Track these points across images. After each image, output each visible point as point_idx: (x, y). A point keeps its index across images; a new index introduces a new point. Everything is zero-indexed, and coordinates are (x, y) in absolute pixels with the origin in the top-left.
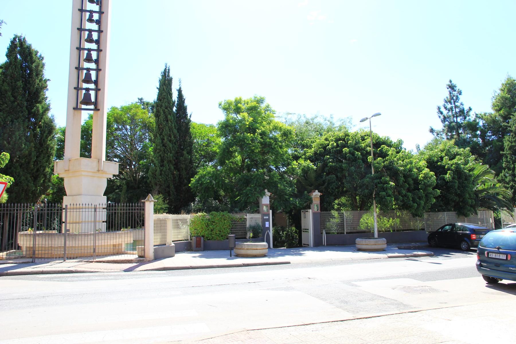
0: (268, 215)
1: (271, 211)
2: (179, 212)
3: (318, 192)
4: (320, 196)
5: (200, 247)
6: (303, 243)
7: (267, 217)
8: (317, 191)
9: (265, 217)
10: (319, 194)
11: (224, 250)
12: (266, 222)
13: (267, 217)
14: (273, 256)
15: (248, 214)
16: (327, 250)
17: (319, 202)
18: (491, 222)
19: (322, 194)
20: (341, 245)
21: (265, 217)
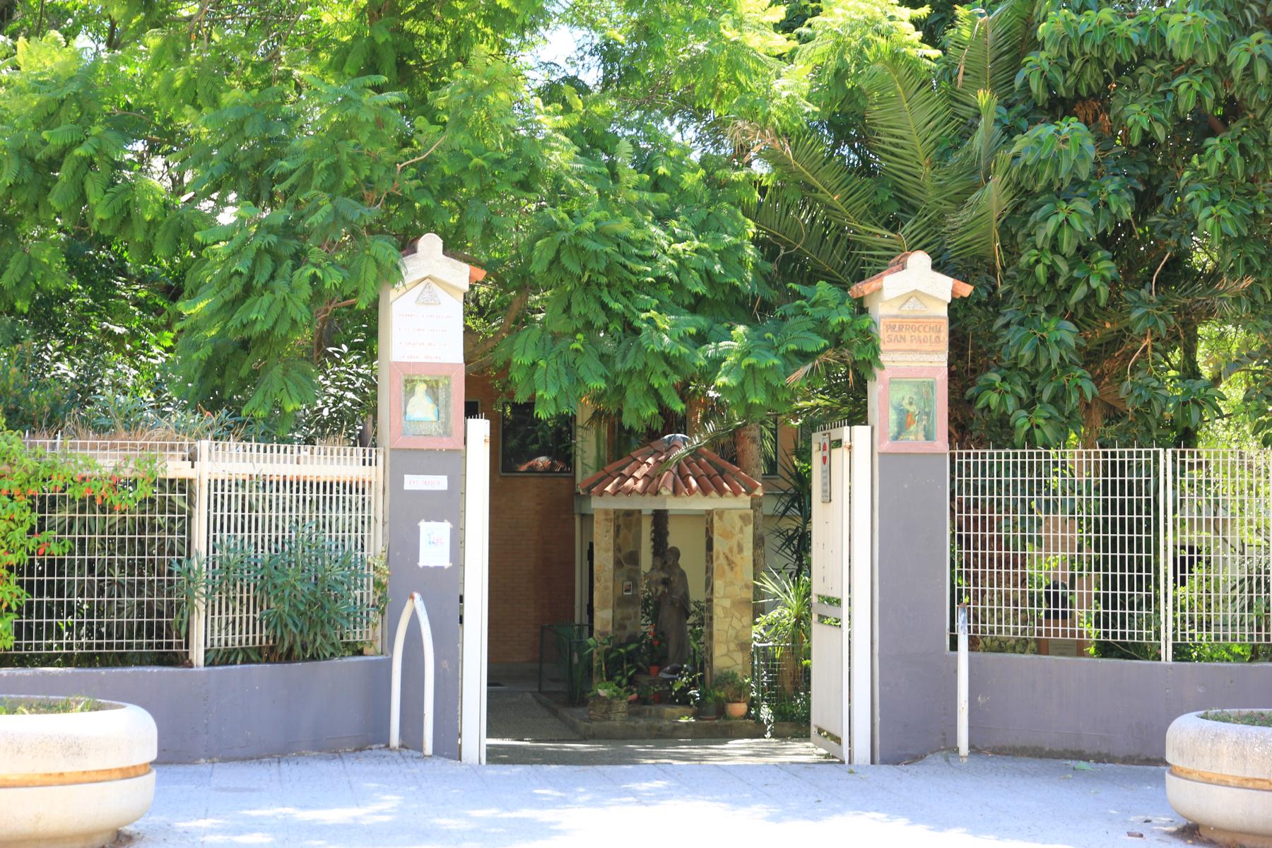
0: (454, 462)
1: (480, 428)
2: (449, 251)
3: (936, 267)
4: (957, 308)
5: (420, 748)
6: (815, 720)
7: (439, 483)
8: (920, 261)
9: (413, 482)
10: (944, 287)
11: (245, 759)
12: (423, 525)
13: (439, 483)
14: (317, 807)
15: (204, 445)
16: (862, 808)
17: (941, 360)
18: (577, 621)
19: (966, 290)
20: (1128, 760)
21: (413, 482)
